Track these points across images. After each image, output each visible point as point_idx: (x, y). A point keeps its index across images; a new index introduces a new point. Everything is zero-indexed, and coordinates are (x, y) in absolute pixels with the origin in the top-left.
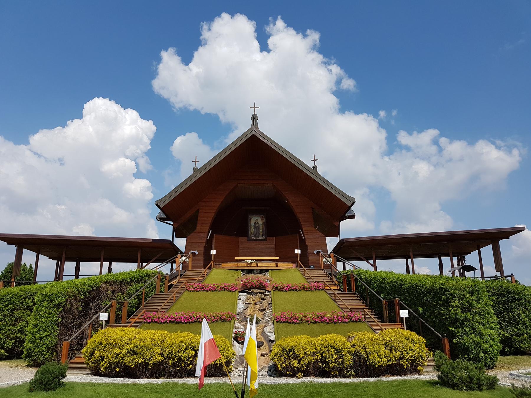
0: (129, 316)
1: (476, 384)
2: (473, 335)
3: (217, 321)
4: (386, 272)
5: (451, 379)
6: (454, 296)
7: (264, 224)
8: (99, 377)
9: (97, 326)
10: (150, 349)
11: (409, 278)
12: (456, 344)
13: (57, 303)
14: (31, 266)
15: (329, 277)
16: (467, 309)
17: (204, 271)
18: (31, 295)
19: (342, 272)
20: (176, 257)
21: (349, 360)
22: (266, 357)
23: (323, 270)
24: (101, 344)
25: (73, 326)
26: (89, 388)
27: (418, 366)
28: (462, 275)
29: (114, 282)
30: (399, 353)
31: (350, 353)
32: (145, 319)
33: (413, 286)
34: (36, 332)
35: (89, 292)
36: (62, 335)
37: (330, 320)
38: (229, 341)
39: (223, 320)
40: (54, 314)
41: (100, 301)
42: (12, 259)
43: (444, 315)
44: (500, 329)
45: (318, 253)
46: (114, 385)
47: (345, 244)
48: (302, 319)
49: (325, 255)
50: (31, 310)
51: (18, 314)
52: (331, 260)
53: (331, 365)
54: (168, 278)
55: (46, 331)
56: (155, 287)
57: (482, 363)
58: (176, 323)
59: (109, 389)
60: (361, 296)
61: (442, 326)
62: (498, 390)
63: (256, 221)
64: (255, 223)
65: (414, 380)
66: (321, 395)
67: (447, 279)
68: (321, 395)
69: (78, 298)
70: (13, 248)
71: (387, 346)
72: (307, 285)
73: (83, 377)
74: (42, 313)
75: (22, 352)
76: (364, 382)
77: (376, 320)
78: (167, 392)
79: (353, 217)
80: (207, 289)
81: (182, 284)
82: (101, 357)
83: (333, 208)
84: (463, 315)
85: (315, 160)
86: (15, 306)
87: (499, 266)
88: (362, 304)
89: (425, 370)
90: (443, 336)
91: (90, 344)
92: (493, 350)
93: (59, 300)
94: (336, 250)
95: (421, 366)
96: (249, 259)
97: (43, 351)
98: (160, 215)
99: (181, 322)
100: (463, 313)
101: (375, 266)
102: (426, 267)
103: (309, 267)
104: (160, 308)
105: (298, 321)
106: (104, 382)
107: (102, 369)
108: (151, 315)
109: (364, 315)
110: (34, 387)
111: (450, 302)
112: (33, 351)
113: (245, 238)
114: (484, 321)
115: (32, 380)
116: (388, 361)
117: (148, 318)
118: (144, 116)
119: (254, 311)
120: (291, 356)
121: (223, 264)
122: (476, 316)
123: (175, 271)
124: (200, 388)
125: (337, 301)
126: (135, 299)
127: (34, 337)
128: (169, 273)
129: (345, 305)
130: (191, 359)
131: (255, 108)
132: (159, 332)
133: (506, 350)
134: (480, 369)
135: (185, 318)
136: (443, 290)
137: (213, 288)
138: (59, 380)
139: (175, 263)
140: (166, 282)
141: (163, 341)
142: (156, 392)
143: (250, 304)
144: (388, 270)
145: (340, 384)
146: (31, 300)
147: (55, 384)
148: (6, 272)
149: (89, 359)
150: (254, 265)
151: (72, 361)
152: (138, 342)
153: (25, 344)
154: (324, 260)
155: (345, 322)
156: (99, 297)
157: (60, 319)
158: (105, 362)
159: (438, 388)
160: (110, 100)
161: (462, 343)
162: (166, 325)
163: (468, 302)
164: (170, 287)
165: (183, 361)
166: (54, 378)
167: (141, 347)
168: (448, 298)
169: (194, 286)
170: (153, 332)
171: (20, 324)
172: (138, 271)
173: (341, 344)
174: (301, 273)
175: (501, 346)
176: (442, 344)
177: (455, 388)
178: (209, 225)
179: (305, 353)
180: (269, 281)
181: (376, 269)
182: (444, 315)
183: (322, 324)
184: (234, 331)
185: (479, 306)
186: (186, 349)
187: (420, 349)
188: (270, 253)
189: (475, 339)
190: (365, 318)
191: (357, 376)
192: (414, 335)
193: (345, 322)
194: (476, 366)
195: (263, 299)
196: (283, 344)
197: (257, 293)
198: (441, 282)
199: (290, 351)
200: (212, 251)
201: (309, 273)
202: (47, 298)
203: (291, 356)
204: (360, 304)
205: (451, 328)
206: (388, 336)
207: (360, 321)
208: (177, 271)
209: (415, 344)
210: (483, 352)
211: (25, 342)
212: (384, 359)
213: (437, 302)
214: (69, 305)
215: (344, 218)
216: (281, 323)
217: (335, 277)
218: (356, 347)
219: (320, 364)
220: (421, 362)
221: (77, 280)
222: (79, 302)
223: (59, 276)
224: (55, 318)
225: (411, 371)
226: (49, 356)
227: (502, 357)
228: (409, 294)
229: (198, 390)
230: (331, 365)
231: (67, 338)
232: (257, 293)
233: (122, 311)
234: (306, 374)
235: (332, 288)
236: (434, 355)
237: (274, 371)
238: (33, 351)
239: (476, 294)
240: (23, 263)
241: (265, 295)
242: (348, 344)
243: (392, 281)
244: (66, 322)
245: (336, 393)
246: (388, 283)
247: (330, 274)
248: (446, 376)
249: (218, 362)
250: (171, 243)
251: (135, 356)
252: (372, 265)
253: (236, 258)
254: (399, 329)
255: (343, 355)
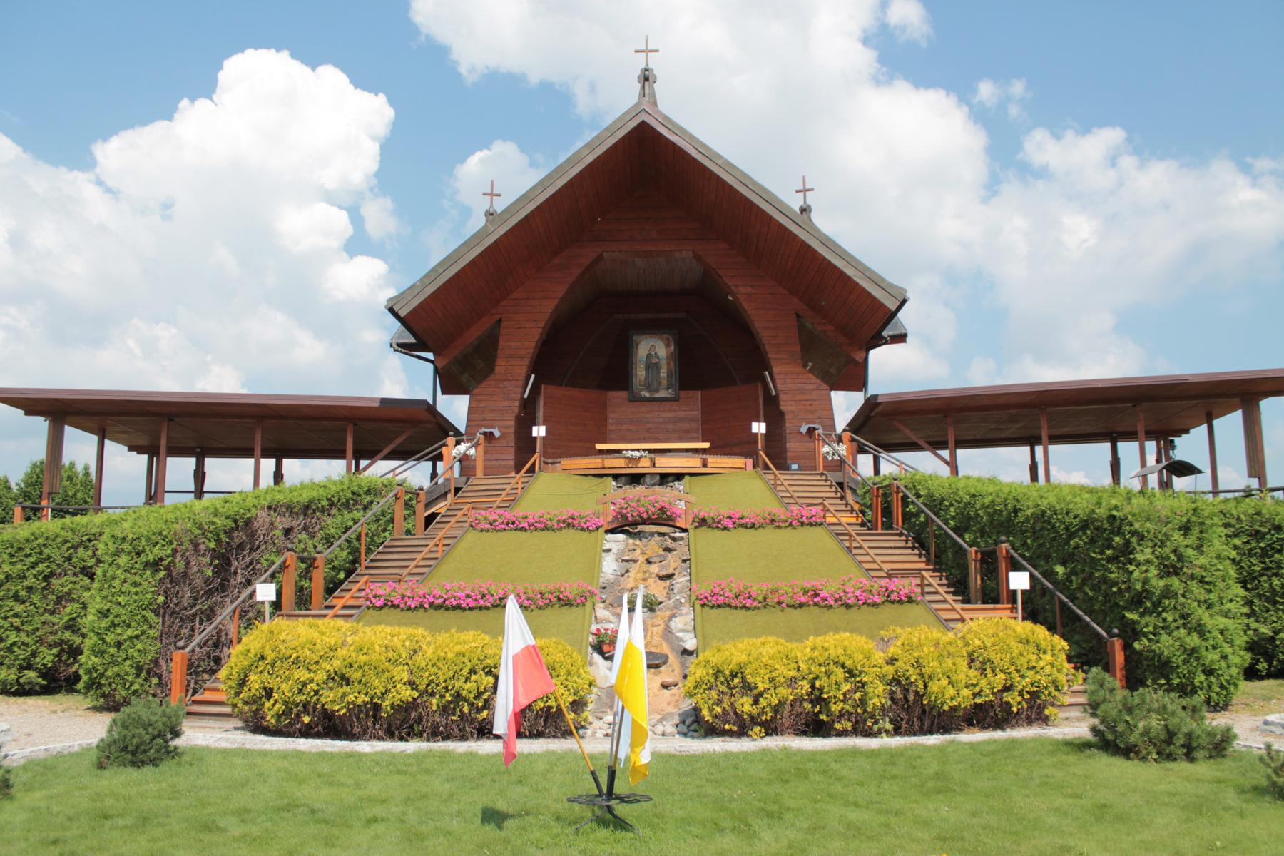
0: (329, 592)
1: (1183, 746)
2: (1182, 631)
3: (549, 604)
4: (979, 480)
5: (1122, 735)
6: (1142, 538)
7: (670, 357)
8: (262, 737)
9: (250, 615)
10: (383, 671)
11: (1035, 494)
12: (1140, 653)
13: (151, 558)
14: (86, 468)
15: (836, 492)
16: (1170, 569)
17: (518, 480)
18: (90, 540)
19: (869, 479)
20: (444, 445)
21: (878, 695)
22: (674, 690)
23: (822, 474)
24: (262, 658)
25: (194, 615)
26: (238, 761)
27: (1045, 707)
28: (1165, 485)
29: (290, 508)
30: (1001, 676)
31: (882, 678)
32: (367, 599)
33: (1044, 512)
34: (107, 629)
35: (230, 533)
36: (170, 637)
37: (836, 600)
38: (580, 652)
39: (566, 603)
40: (145, 585)
41: (256, 555)
42: (39, 451)
43: (1116, 584)
44: (1248, 616)
45: (811, 431)
46: (298, 754)
47: (880, 408)
48: (765, 599)
49: (829, 436)
50: (92, 577)
51: (62, 585)
52: (843, 449)
53: (835, 708)
54: (422, 497)
55: (129, 626)
56: (392, 521)
57: (1200, 697)
58: (447, 609)
59: (286, 764)
60: (916, 539)
61: (1110, 610)
62: (1234, 760)
63: (653, 350)
64: (649, 356)
65: (1034, 740)
66: (806, 778)
67: (1129, 495)
68: (806, 778)
69: (202, 547)
70: (40, 425)
71: (972, 661)
72: (781, 514)
73: (224, 735)
74: (116, 583)
75: (77, 678)
76: (913, 747)
77: (950, 598)
78: (428, 772)
79: (900, 338)
80: (524, 524)
81: (460, 513)
82: (265, 688)
83: (849, 318)
84: (1162, 583)
85: (805, 191)
86: (54, 566)
87: (1256, 464)
88: (916, 558)
89: (1062, 715)
90: (1111, 635)
91: (235, 657)
92: (1229, 667)
93: (156, 550)
94: (857, 425)
95: (1053, 705)
96: (632, 449)
97: (127, 673)
98: (401, 336)
99: (458, 607)
100: (1162, 578)
101: (953, 465)
102: (1078, 469)
103: (788, 468)
104: (405, 571)
105: (756, 604)
106: (275, 747)
107: (269, 718)
108: (383, 589)
109: (921, 585)
110: (108, 757)
111: (1131, 552)
112: (102, 675)
113: (623, 394)
114: (1212, 596)
115: (102, 740)
116: (975, 695)
117: (375, 597)
118: (361, 80)
119: (645, 579)
120: (735, 687)
121: (567, 462)
122: (1194, 585)
123: (441, 481)
124: (507, 762)
125: (854, 551)
126: (342, 550)
127: (103, 640)
128: (426, 484)
129: (874, 562)
130: (485, 696)
131: (647, 51)
132: (405, 632)
133: (1260, 667)
134: (1194, 710)
135: (468, 596)
136: (1115, 523)
137: (540, 522)
138: (166, 741)
139: (441, 459)
140: (420, 507)
141: (415, 652)
142: (399, 772)
143: (635, 561)
144: (985, 474)
145: (855, 752)
146: (90, 553)
147: (158, 751)
148: (28, 485)
149: (237, 694)
150: (645, 462)
151: (197, 697)
152: (354, 654)
153: (82, 658)
154: (826, 449)
155: (874, 605)
156: (252, 544)
157: (161, 599)
158: (276, 701)
159: (1089, 757)
160: (278, 51)
161: (1154, 651)
162: (421, 613)
163: (1175, 551)
164: (430, 520)
165: (466, 700)
166: (154, 738)
167: (360, 667)
168: (1128, 543)
169: (491, 518)
170: (388, 629)
171: (68, 610)
172: (346, 480)
173: (861, 657)
174: (766, 482)
175: (1248, 657)
176: (1108, 655)
177: (1132, 755)
178: (527, 362)
179: (772, 680)
180: (683, 503)
181: (955, 470)
182: (1116, 584)
183: (816, 610)
184: (594, 628)
185: (1203, 560)
186: (473, 671)
187: (1052, 665)
188: (688, 432)
189: (1188, 639)
190: (923, 594)
191: (897, 731)
192: (1041, 632)
193: (874, 605)
194: (1184, 703)
195: (668, 550)
196: (716, 659)
197: (652, 534)
198: (1114, 502)
199: (734, 676)
200: (535, 429)
201: (786, 483)
202: (126, 546)
203: (735, 687)
204: (913, 560)
205: (1129, 615)
206: (977, 635)
207: (910, 601)
208: (447, 480)
209: (1044, 653)
210: (1203, 671)
211: (81, 653)
212: (965, 692)
213: (1102, 553)
214: (180, 565)
215: (877, 340)
216: (712, 607)
217: (854, 491)
218: (898, 664)
219: (807, 706)
220: (1055, 697)
221: (197, 502)
222: (204, 556)
223: (154, 494)
224: (149, 596)
225: (1028, 717)
226: (142, 685)
227: (1250, 684)
228: (1034, 533)
229: (503, 768)
230: (835, 708)
231: (181, 644)
232: (652, 534)
233: (311, 580)
234: (771, 729)
235: (844, 520)
236: (1085, 680)
237: (696, 724)
238: (102, 675)
239: (1195, 531)
240: (66, 460)
241: (674, 539)
242: (879, 657)
243: (993, 501)
244: (176, 605)
245: (844, 772)
246: (983, 507)
247: (841, 485)
248: (1112, 728)
249: (552, 703)
250: (431, 409)
251: (346, 689)
252: (947, 463)
253: (599, 446)
254: (1005, 619)
255: (864, 684)
